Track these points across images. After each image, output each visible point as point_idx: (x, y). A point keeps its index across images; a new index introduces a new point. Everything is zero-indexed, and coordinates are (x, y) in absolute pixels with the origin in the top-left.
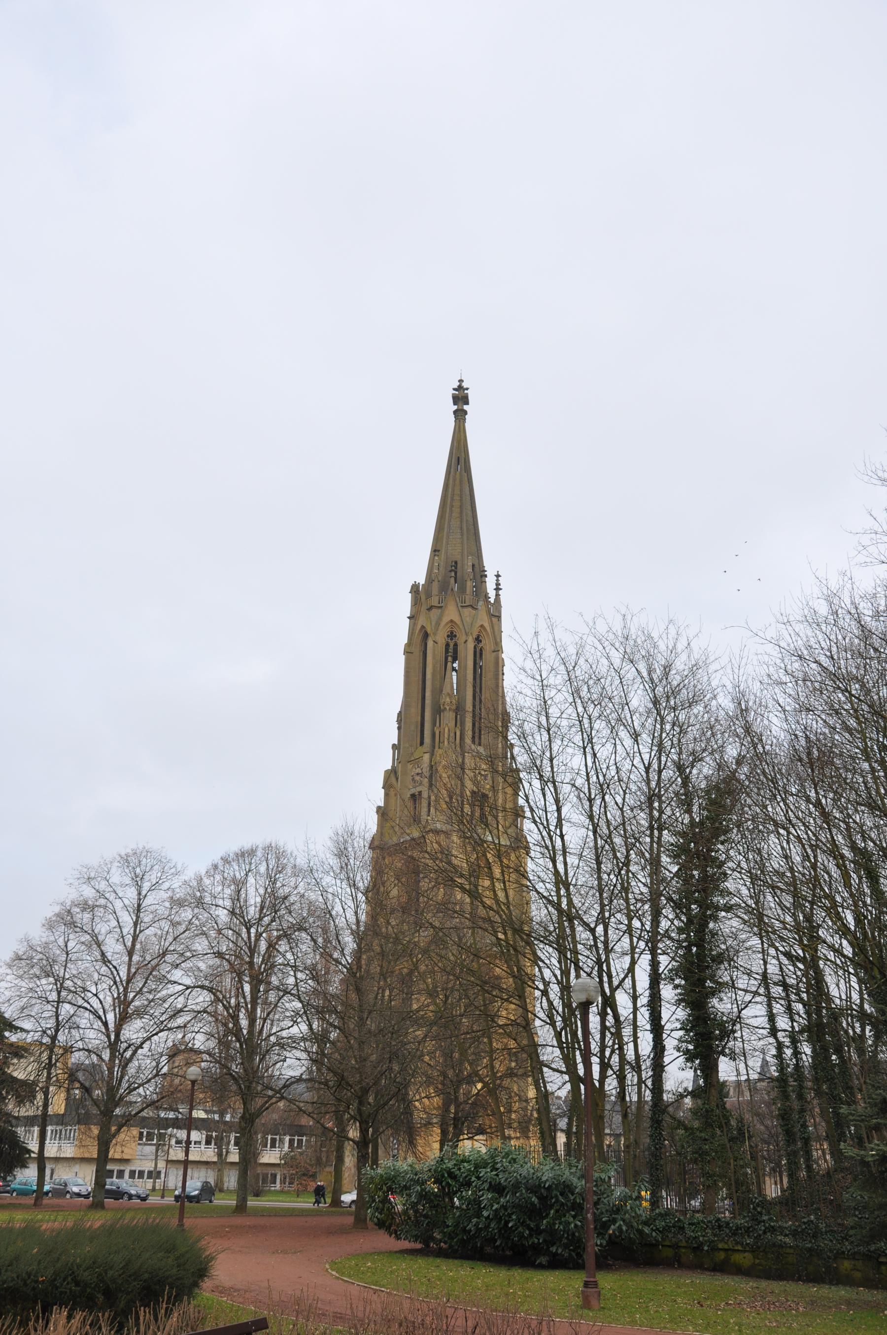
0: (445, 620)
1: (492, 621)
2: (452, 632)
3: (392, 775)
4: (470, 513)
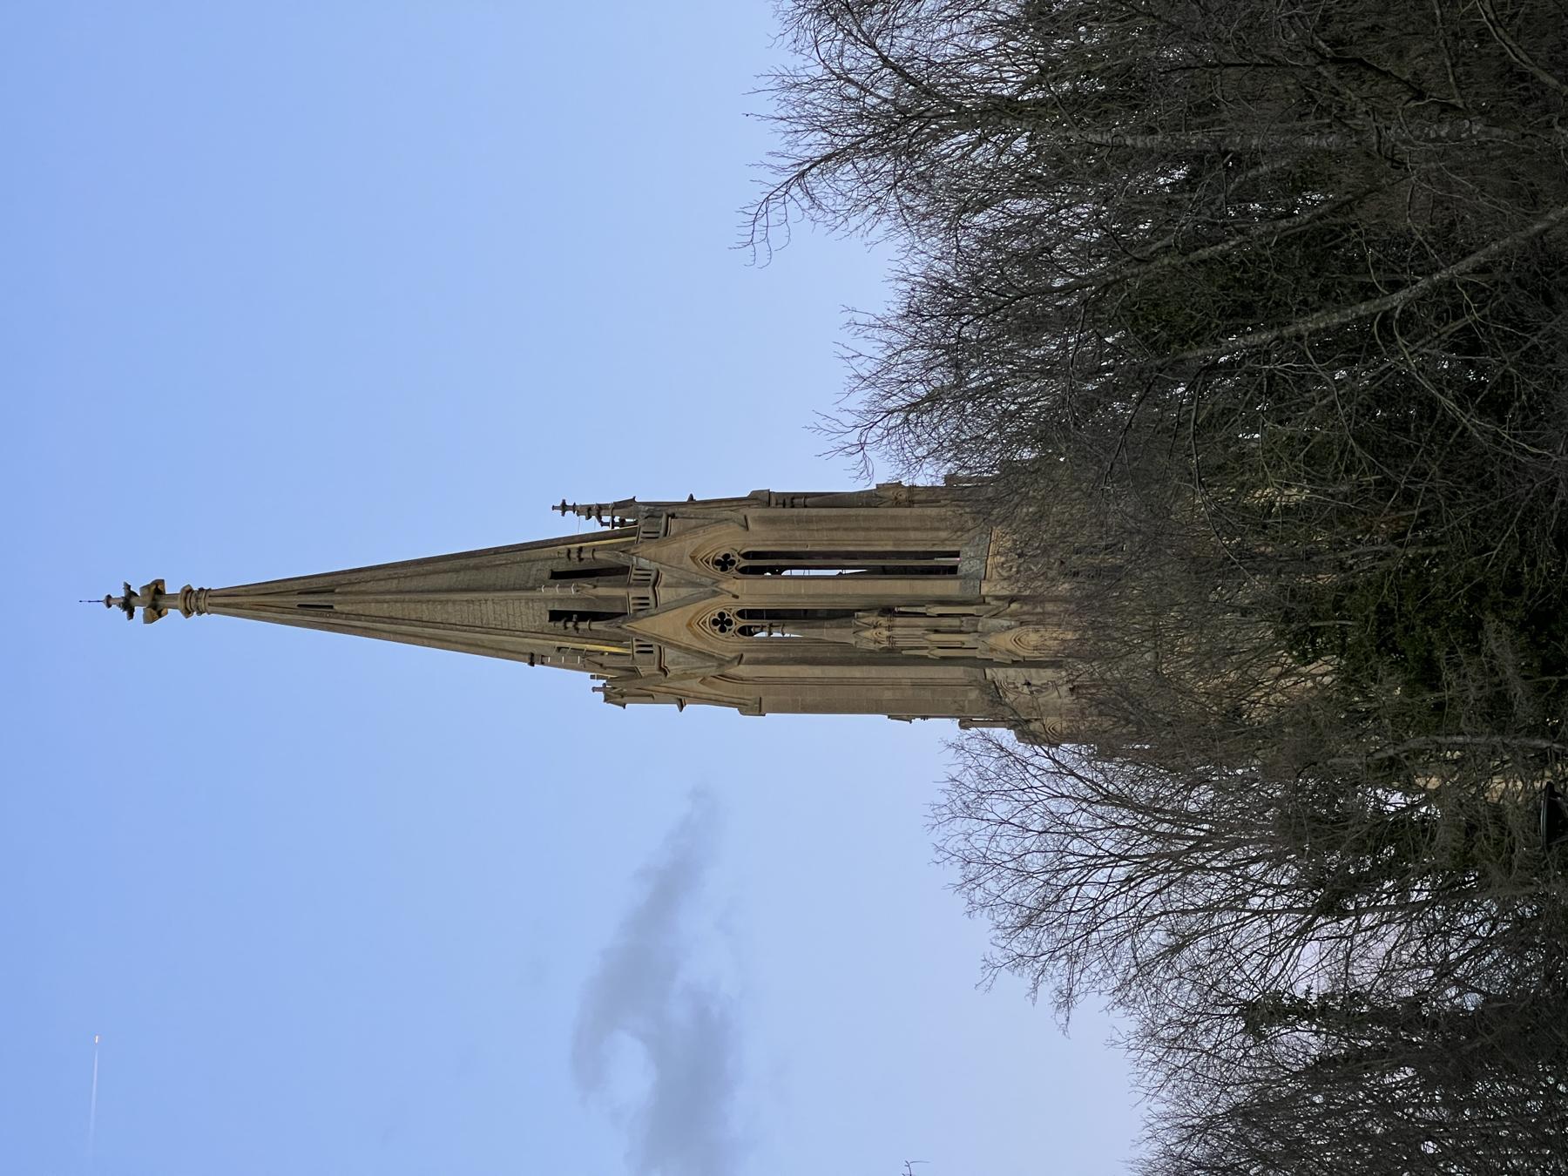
0: (686, 639)
2: (715, 622)
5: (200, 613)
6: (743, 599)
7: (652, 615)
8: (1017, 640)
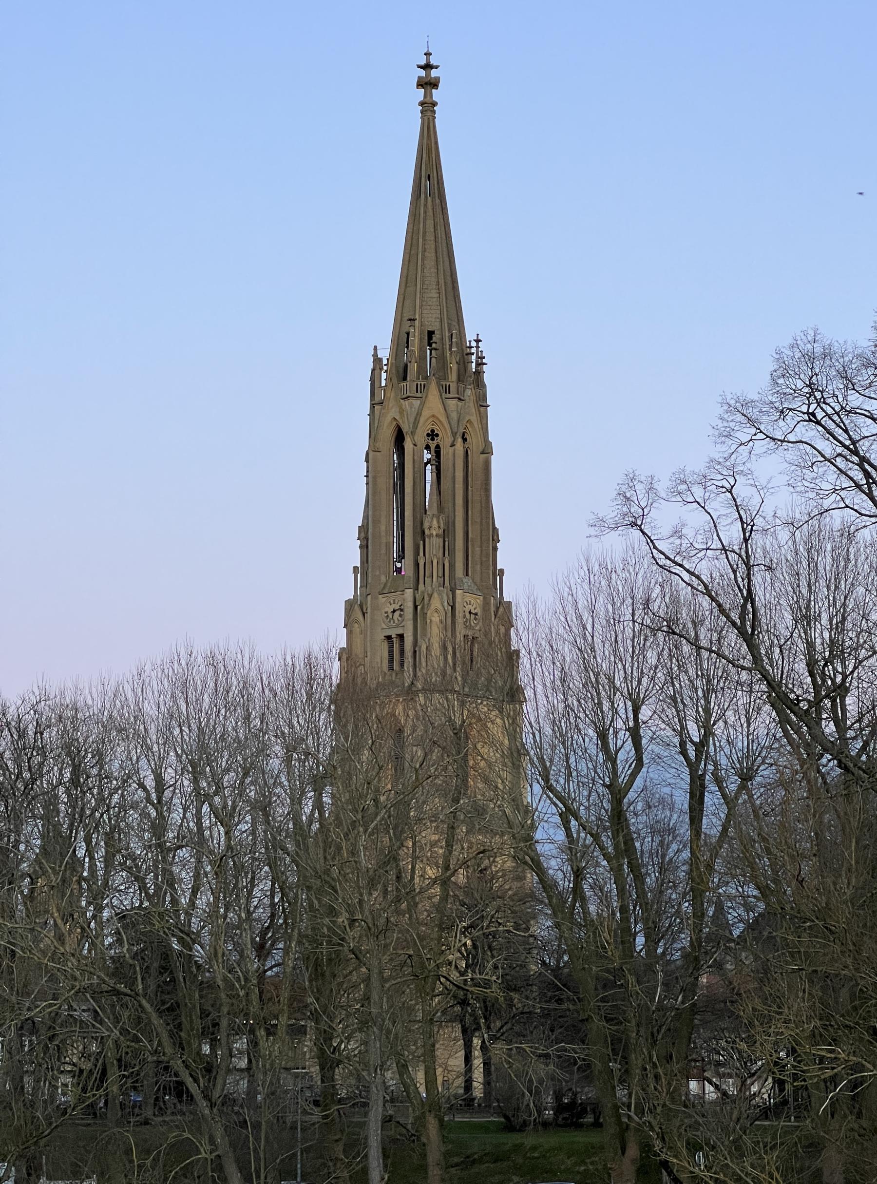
0: (426, 413)
1: (479, 411)
2: (433, 431)
3: (357, 608)
4: (446, 259)
5: (422, 113)
6: (451, 450)
7: (441, 395)
8: (436, 611)
